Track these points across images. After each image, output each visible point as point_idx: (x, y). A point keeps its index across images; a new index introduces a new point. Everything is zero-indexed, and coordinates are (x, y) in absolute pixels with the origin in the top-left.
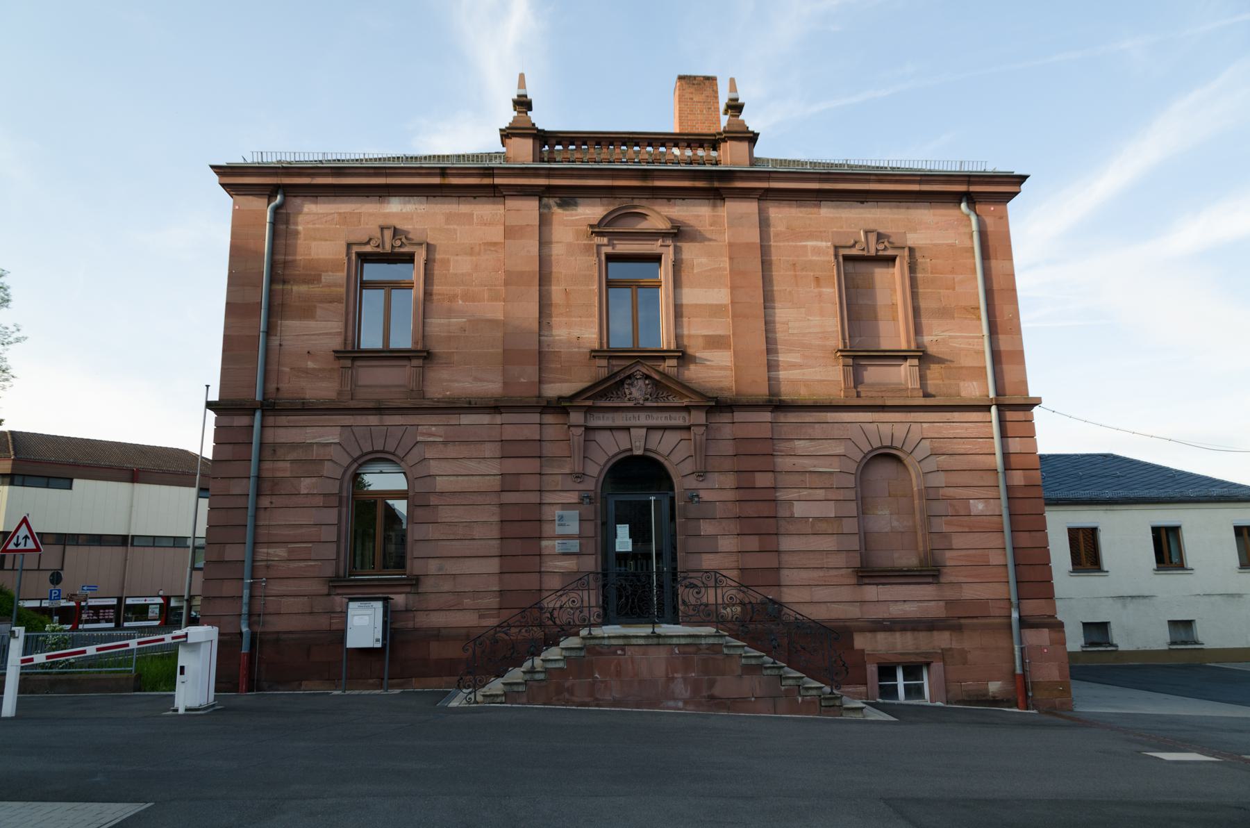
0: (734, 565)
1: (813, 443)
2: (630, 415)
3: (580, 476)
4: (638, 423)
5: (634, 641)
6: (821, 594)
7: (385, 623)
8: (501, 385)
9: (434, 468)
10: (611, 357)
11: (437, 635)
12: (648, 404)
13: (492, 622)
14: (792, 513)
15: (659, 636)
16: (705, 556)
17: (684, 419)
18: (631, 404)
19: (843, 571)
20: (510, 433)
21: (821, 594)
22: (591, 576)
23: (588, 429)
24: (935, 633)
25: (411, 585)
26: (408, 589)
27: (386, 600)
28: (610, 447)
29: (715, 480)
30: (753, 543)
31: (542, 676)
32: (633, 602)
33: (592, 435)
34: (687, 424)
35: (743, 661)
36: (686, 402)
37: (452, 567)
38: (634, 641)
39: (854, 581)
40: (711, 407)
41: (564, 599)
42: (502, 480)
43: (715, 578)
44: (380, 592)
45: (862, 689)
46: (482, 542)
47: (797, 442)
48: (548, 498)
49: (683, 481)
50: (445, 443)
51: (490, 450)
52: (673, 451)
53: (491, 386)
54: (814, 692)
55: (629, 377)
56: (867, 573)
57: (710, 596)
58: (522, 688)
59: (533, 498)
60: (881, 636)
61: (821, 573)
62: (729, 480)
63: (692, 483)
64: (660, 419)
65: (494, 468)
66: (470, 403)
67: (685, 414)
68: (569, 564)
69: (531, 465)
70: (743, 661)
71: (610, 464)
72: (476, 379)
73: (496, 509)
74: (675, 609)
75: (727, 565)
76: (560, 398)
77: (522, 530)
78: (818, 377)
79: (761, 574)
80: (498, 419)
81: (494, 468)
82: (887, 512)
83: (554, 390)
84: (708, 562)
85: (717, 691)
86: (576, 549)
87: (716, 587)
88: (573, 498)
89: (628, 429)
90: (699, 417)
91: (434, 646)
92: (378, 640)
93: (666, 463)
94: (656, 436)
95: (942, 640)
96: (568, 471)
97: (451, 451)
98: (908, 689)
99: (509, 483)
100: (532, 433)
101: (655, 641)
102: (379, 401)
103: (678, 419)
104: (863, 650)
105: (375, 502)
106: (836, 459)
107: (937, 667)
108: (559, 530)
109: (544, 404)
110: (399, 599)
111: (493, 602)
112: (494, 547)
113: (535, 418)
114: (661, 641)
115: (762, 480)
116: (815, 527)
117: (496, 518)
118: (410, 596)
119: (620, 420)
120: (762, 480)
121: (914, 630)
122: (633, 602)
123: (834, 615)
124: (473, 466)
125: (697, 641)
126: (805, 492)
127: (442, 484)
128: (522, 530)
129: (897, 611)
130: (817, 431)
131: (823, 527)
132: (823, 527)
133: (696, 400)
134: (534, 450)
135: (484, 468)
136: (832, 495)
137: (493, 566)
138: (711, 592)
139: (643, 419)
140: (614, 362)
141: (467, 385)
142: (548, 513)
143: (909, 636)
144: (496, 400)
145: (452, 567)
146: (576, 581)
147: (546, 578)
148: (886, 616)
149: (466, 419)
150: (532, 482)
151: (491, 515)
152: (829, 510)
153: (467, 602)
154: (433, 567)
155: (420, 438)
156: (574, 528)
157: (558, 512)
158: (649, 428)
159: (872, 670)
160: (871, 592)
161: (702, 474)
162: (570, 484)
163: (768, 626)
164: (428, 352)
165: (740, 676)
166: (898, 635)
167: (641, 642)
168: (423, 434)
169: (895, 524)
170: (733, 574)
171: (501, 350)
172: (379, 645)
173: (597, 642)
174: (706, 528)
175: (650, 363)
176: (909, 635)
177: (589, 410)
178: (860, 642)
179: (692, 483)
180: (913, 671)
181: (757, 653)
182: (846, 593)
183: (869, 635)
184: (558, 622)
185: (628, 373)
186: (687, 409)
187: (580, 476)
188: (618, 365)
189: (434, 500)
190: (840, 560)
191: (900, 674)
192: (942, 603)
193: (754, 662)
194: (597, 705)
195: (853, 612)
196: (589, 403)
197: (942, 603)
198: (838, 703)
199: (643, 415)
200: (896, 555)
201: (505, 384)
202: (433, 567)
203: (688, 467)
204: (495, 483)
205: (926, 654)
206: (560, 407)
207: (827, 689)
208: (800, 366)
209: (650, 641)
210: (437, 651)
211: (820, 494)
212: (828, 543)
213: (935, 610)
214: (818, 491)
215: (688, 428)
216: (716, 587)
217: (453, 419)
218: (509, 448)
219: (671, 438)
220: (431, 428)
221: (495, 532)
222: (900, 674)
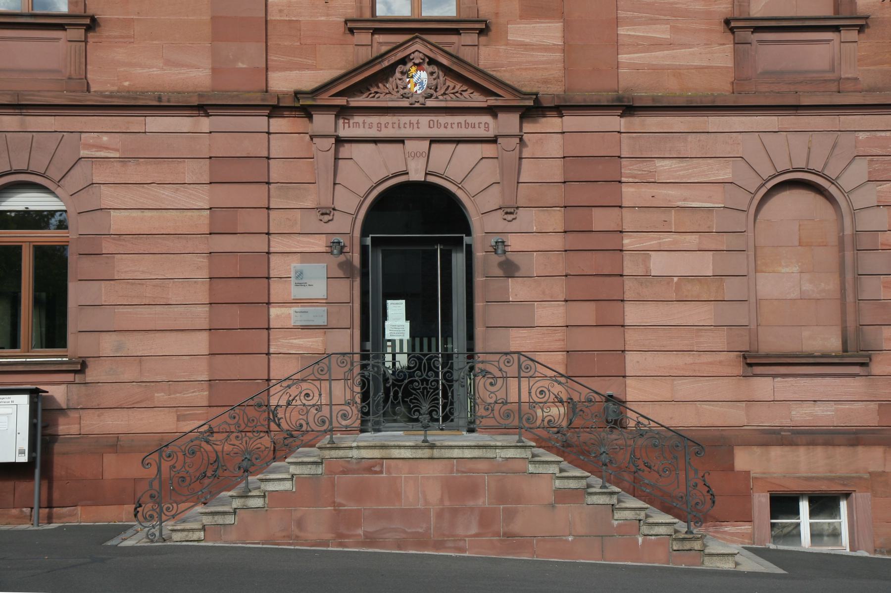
0: (558, 345)
1: (684, 164)
2: (405, 119)
3: (326, 212)
4: (416, 132)
5: (396, 453)
6: (686, 389)
7: (33, 427)
8: (208, 72)
9: (108, 197)
10: (376, 31)
11: (115, 444)
12: (430, 103)
13: (187, 426)
14: (648, 269)
15: (432, 447)
16: (513, 332)
17: (487, 127)
18: (405, 103)
19: (722, 357)
20: (223, 146)
21: (686, 389)
22: (334, 358)
23: (340, 141)
24: (860, 449)
25: (75, 372)
26: (70, 377)
27: (34, 394)
28: (371, 169)
29: (527, 218)
30: (586, 313)
31: (259, 502)
32: (396, 393)
33: (346, 150)
34: (491, 134)
35: (558, 483)
36: (492, 101)
37: (136, 345)
38: (396, 453)
39: (740, 370)
40: (528, 108)
41: (294, 391)
42: (211, 217)
43: (524, 363)
44: (29, 382)
45: (746, 528)
46: (181, 309)
47: (659, 163)
48: (278, 244)
49: (484, 224)
50: (124, 160)
51: (199, 171)
52: (466, 172)
53: (194, 75)
54: (662, 530)
55: (403, 61)
56: (754, 362)
57: (515, 391)
58: (230, 519)
59: (258, 244)
60: (776, 452)
61: (688, 359)
62: (555, 220)
63: (496, 222)
64: (453, 126)
65: (201, 198)
66: (160, 99)
67: (487, 119)
68: (313, 343)
69: (253, 195)
70: (558, 483)
71: (375, 193)
72: (168, 63)
73: (203, 261)
74: (448, 404)
75: (546, 346)
76: (297, 94)
77: (241, 293)
78: (697, 63)
79: (595, 361)
80: (205, 123)
81: (201, 198)
82: (796, 269)
83: (283, 82)
84: (519, 340)
85: (517, 526)
86: (322, 321)
87: (519, 377)
88: (319, 244)
89: (401, 141)
90: (510, 122)
91: (110, 460)
92: (22, 452)
93: (459, 194)
94: (441, 152)
95: (871, 459)
96: (309, 204)
97: (133, 173)
98: (816, 535)
99: (222, 222)
100: (254, 146)
101: (427, 453)
102: (18, 94)
103: (483, 125)
104: (748, 473)
105: (20, 247)
106: (719, 188)
107: (861, 497)
108: (297, 293)
109: (274, 102)
110: (58, 392)
111: (201, 396)
112: (201, 315)
113: (259, 122)
114: (436, 453)
115: (602, 220)
116: (681, 290)
117: (205, 274)
118: (74, 388)
119: (388, 126)
120: (602, 220)
121: (826, 444)
122: (396, 393)
123: (706, 421)
124: (167, 196)
125: (490, 453)
126: (667, 239)
127: (119, 222)
128: (241, 293)
129: (801, 416)
130: (692, 146)
131: (694, 290)
132: (694, 290)
133: (508, 99)
134: (253, 171)
135: (182, 198)
136: (710, 242)
137: (200, 343)
138: (513, 383)
139: (424, 125)
140: (379, 38)
141: (155, 71)
142: (277, 266)
143: (819, 452)
144: (201, 96)
145: (136, 345)
146: (318, 366)
147: (275, 362)
148: (786, 422)
149: (157, 123)
150: (255, 221)
151: (198, 269)
152: (705, 265)
153: (160, 397)
154: (108, 344)
155: (84, 153)
156: (318, 289)
157: (295, 265)
158: (434, 141)
159: (761, 502)
160: (764, 387)
161: (509, 211)
162: (313, 222)
163: (599, 437)
164: (93, 19)
165: (552, 506)
166: (802, 450)
167: (407, 453)
168: (89, 146)
169: (807, 287)
170: (557, 361)
171: (206, 18)
172: (24, 459)
173: (341, 453)
174: (517, 289)
175: (433, 38)
176: (819, 451)
177: (343, 112)
178: (745, 460)
179: (496, 222)
180: (824, 504)
181: (578, 473)
182: (725, 389)
183: (757, 450)
184: (284, 426)
185: (400, 55)
186: (492, 111)
187: (326, 212)
188: (384, 41)
189: (107, 246)
190: (718, 340)
191: (804, 506)
192: (873, 406)
193: (573, 484)
194: (341, 545)
195: (734, 417)
196: (341, 101)
197: (873, 406)
198: (697, 545)
199: (424, 119)
200: (806, 333)
201: (214, 70)
202: (108, 344)
203: (492, 199)
204: (202, 221)
205: (843, 479)
206: (301, 106)
207: (682, 526)
208: (669, 45)
209: (419, 453)
210: (114, 468)
211: (692, 241)
212: (701, 314)
213: (864, 415)
214: (688, 237)
215: (493, 141)
216: (519, 377)
217: (134, 123)
218: (224, 171)
219: (469, 153)
220: (100, 134)
221: (202, 295)
222: (804, 506)
